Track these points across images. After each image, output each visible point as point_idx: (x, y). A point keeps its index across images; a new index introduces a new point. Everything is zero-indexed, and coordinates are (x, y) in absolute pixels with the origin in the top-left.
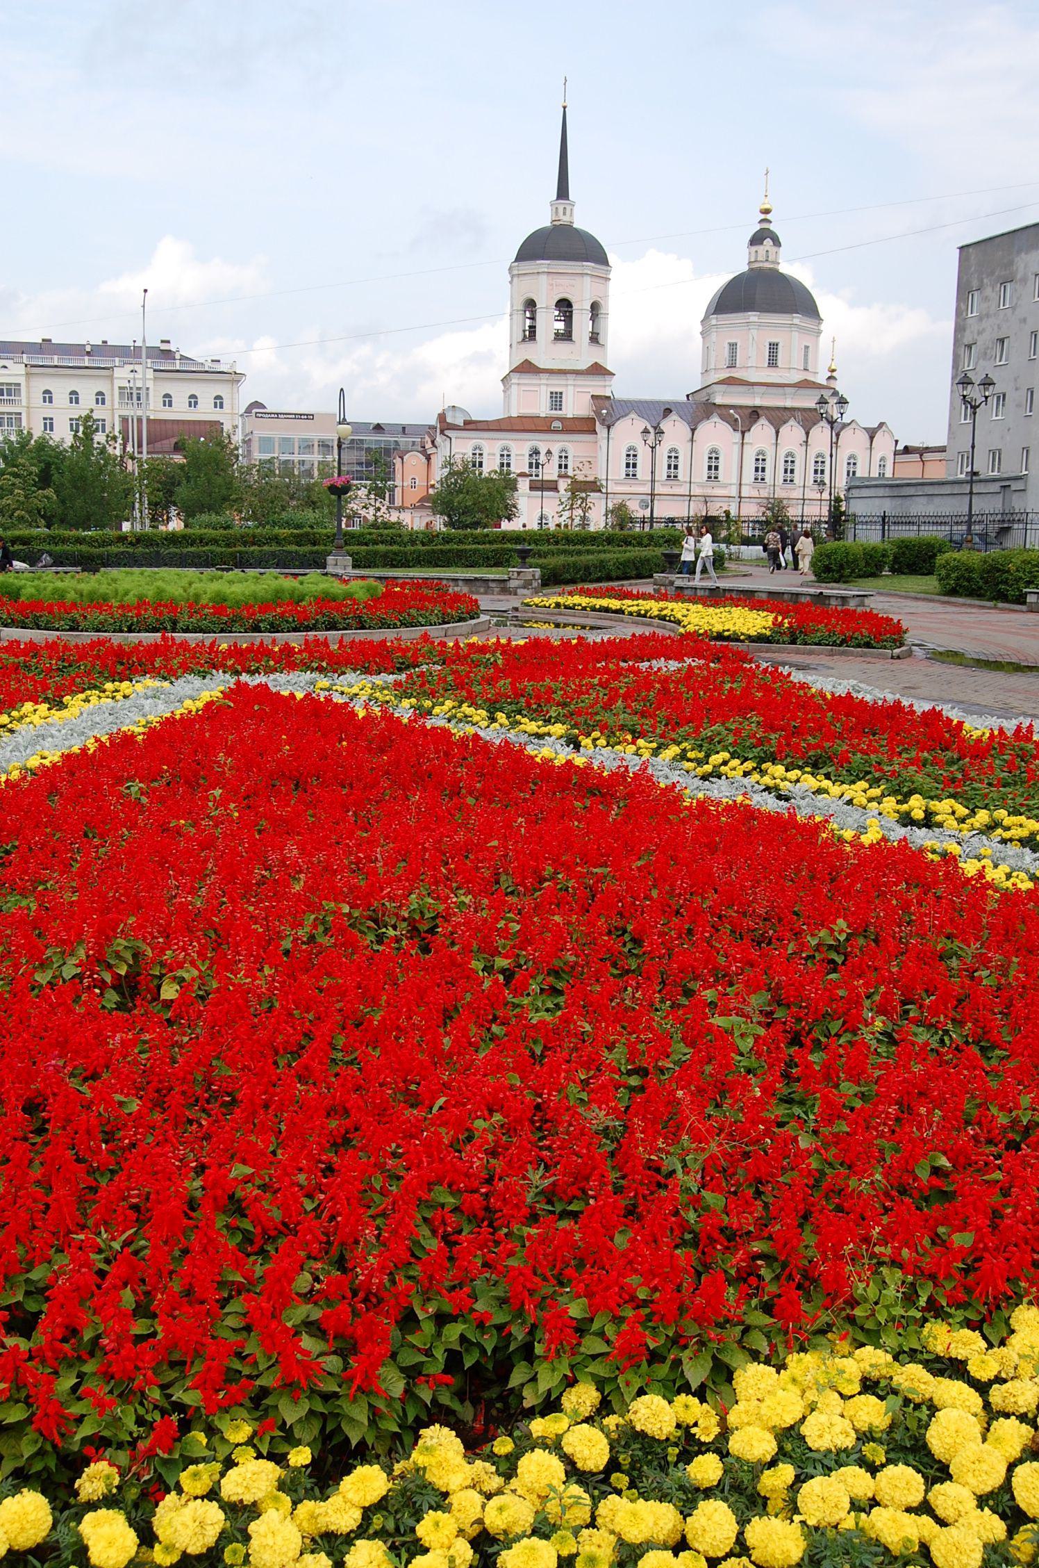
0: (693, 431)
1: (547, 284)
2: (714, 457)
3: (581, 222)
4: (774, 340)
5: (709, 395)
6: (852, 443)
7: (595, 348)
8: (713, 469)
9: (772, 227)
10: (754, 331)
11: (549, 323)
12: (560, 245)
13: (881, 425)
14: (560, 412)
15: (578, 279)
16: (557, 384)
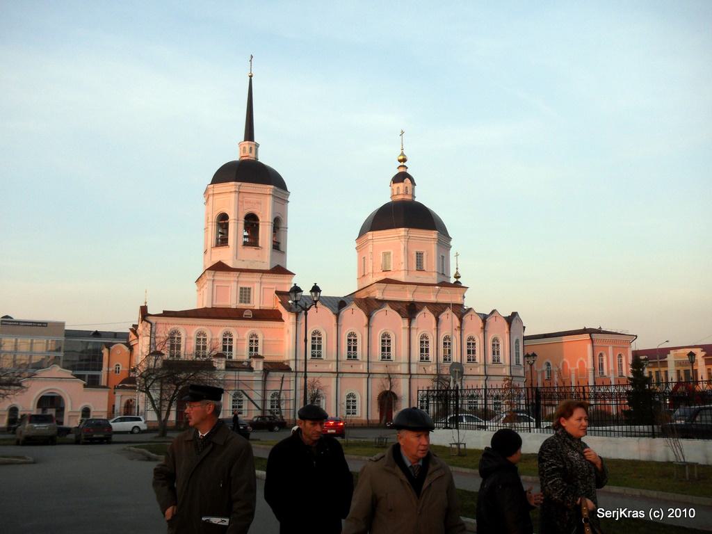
0: (337, 315)
1: (230, 199)
2: (386, 340)
3: (264, 158)
4: (420, 250)
5: (368, 293)
6: (473, 327)
7: (277, 254)
8: (386, 349)
9: (409, 171)
10: (395, 240)
11: (236, 231)
12: (247, 171)
13: (493, 312)
14: (248, 305)
15: (263, 197)
16: (247, 280)
